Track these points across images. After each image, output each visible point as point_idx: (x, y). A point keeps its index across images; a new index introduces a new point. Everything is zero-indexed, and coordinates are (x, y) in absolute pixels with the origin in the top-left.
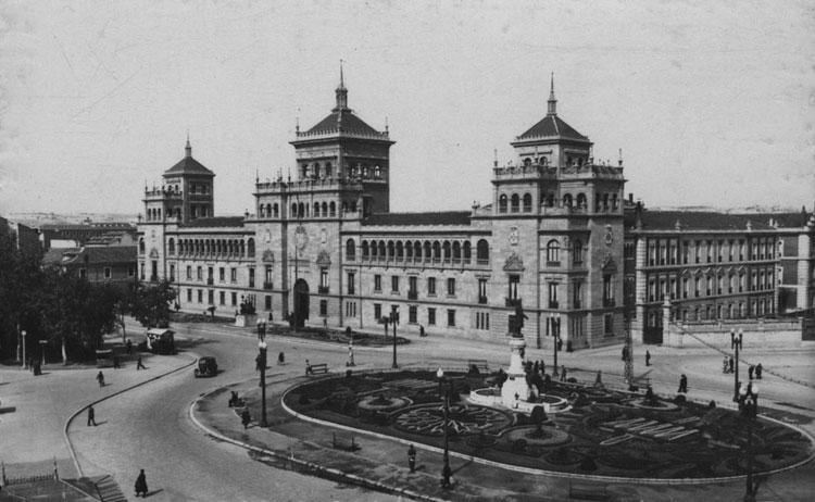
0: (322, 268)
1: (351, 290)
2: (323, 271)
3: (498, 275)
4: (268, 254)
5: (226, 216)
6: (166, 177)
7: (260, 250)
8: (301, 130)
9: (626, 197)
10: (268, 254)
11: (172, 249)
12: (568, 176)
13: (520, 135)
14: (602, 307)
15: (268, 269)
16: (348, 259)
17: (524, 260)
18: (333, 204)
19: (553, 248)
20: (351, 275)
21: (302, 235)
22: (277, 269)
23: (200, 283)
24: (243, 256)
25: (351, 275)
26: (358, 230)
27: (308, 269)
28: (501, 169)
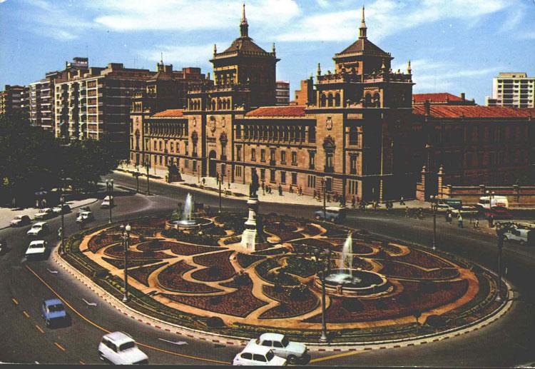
1: (239, 159)
2: (224, 145)
3: (320, 151)
4: (194, 135)
5: (431, 93)
6: (337, 60)
7: (190, 131)
8: (217, 52)
10: (194, 135)
11: (147, 130)
12: (369, 81)
13: (339, 52)
14: (323, 172)
16: (351, 143)
17: (336, 140)
18: (229, 100)
20: (239, 148)
21: (213, 122)
22: (199, 144)
23: (263, 164)
24: (303, 141)
25: (239, 148)
26: (318, 115)
27: (214, 144)
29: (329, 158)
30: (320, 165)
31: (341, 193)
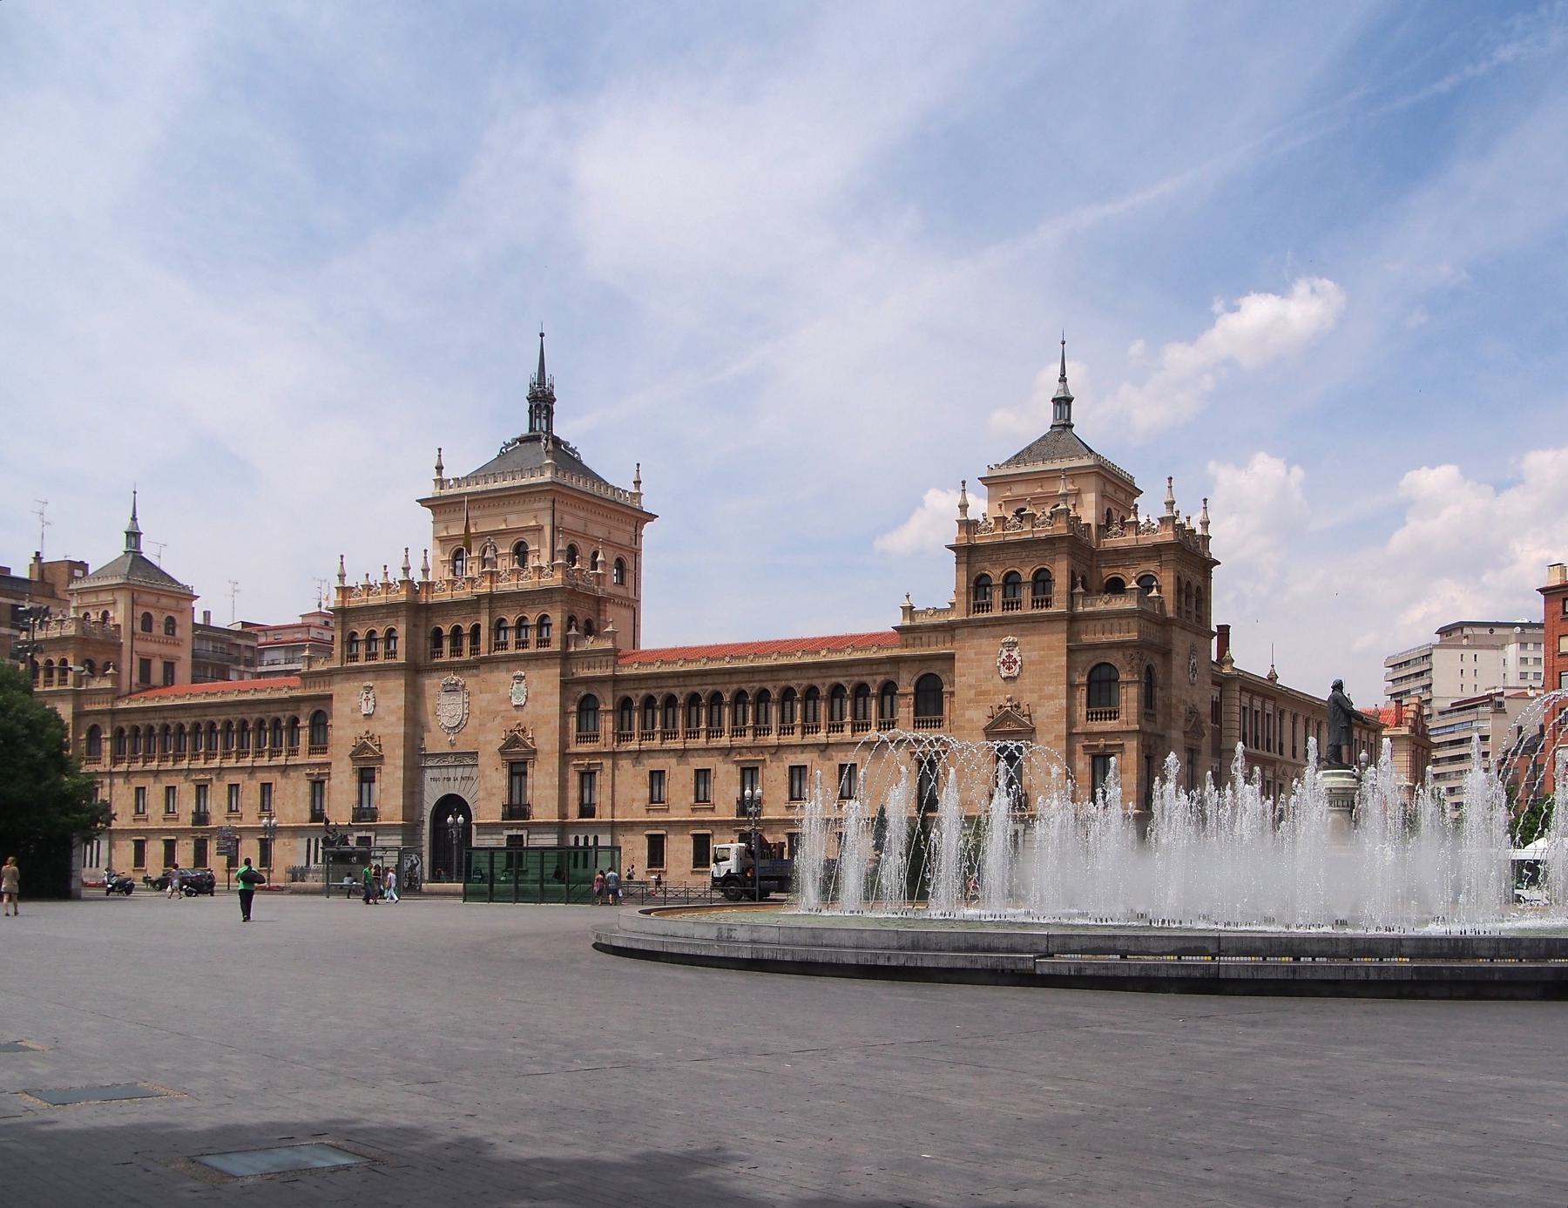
0: (512, 764)
1: (587, 810)
9: (199, 619)
15: (366, 776)
16: (1091, 716)
19: (1100, 682)
20: (587, 776)
28: (351, 589)
29: (365, 786)
30: (340, 810)
31: (486, 871)
